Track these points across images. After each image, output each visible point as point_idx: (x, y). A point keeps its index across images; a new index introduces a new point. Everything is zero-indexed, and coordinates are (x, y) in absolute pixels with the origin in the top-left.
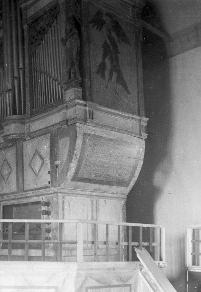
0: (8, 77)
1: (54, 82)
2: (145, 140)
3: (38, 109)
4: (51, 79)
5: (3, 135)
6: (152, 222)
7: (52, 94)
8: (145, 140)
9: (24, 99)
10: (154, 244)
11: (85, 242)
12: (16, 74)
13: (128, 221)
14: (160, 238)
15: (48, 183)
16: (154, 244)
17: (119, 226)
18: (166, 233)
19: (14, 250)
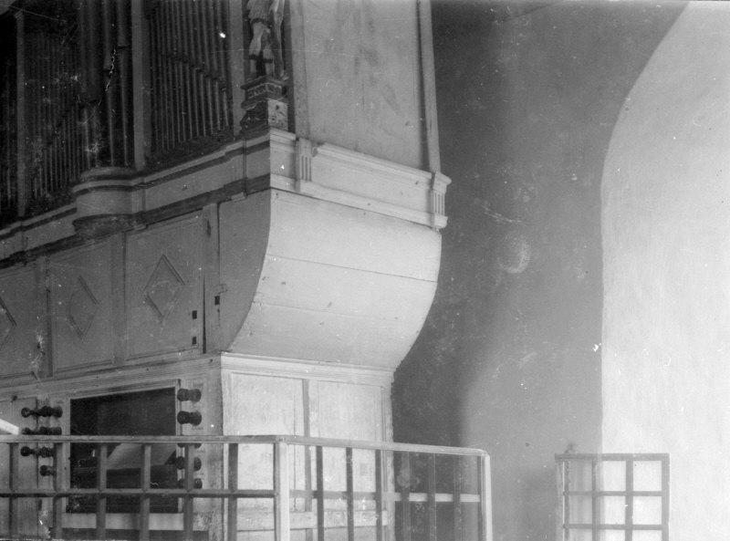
0: (123, 378)
1: (216, 68)
2: (442, 231)
3: (165, 152)
4: (202, 76)
5: (73, 217)
6: (456, 442)
7: (203, 103)
8: (442, 231)
9: (129, 149)
10: (467, 498)
11: (294, 493)
12: (109, 63)
13: (398, 438)
14: (479, 476)
15: (182, 379)
16: (467, 498)
17: (378, 453)
18: (493, 471)
19: (374, 455)
